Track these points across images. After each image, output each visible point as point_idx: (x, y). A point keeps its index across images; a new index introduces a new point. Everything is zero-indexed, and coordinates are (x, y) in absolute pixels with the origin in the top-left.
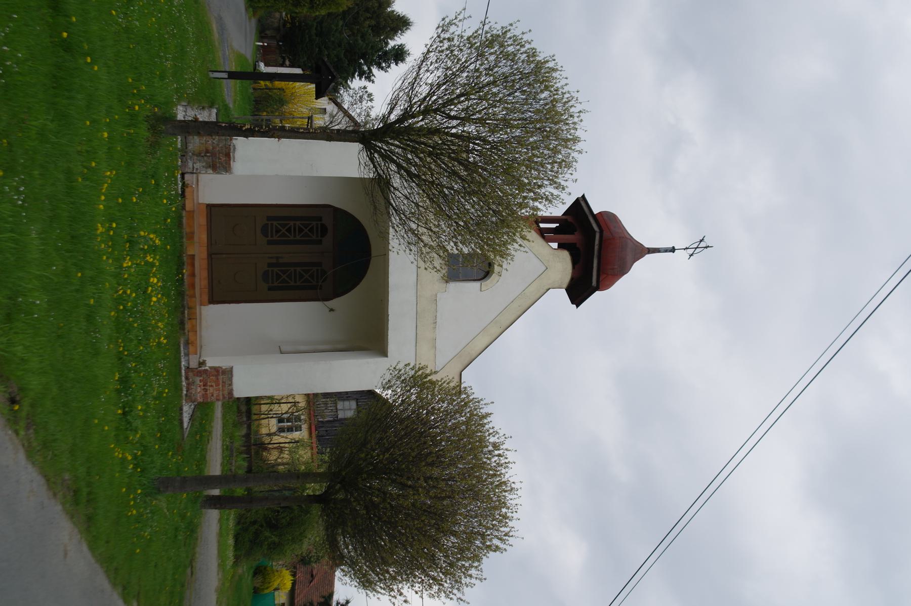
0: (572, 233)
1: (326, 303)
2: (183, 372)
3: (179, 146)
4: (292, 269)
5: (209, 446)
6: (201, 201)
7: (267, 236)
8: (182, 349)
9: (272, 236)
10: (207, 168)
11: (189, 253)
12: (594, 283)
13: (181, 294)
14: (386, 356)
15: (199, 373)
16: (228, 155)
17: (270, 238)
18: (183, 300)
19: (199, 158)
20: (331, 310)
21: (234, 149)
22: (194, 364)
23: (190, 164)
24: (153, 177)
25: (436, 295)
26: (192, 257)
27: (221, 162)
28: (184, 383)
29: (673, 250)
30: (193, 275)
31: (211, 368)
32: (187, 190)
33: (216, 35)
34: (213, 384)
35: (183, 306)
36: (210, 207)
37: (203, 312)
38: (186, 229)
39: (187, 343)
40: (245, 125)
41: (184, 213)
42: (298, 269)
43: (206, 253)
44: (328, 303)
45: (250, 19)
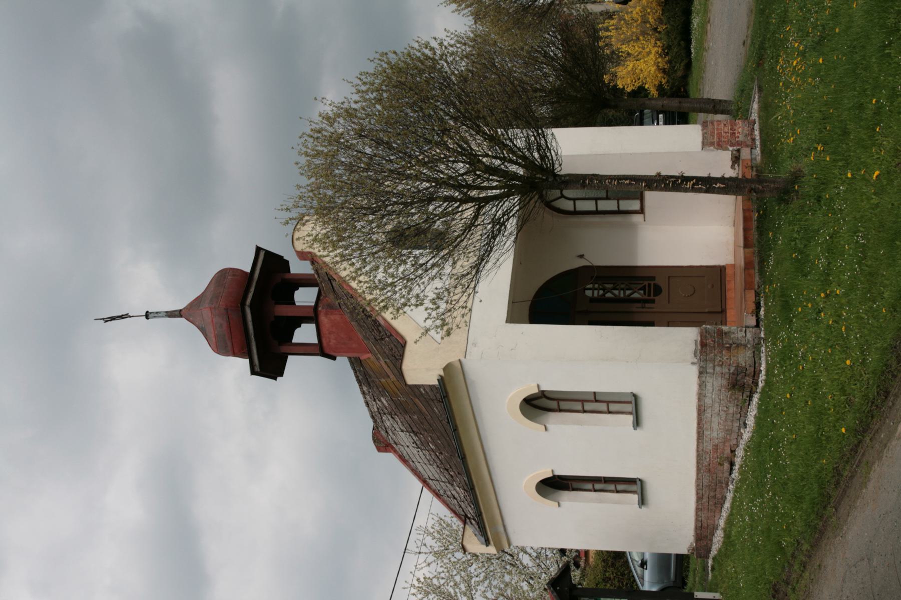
1: (588, 264)
7: (654, 284)
9: (649, 285)
10: (729, 332)
14: (512, 318)
17: (652, 283)
20: (582, 256)
23: (749, 335)
29: (147, 315)
31: (727, 149)
34: (723, 134)
43: (728, 315)
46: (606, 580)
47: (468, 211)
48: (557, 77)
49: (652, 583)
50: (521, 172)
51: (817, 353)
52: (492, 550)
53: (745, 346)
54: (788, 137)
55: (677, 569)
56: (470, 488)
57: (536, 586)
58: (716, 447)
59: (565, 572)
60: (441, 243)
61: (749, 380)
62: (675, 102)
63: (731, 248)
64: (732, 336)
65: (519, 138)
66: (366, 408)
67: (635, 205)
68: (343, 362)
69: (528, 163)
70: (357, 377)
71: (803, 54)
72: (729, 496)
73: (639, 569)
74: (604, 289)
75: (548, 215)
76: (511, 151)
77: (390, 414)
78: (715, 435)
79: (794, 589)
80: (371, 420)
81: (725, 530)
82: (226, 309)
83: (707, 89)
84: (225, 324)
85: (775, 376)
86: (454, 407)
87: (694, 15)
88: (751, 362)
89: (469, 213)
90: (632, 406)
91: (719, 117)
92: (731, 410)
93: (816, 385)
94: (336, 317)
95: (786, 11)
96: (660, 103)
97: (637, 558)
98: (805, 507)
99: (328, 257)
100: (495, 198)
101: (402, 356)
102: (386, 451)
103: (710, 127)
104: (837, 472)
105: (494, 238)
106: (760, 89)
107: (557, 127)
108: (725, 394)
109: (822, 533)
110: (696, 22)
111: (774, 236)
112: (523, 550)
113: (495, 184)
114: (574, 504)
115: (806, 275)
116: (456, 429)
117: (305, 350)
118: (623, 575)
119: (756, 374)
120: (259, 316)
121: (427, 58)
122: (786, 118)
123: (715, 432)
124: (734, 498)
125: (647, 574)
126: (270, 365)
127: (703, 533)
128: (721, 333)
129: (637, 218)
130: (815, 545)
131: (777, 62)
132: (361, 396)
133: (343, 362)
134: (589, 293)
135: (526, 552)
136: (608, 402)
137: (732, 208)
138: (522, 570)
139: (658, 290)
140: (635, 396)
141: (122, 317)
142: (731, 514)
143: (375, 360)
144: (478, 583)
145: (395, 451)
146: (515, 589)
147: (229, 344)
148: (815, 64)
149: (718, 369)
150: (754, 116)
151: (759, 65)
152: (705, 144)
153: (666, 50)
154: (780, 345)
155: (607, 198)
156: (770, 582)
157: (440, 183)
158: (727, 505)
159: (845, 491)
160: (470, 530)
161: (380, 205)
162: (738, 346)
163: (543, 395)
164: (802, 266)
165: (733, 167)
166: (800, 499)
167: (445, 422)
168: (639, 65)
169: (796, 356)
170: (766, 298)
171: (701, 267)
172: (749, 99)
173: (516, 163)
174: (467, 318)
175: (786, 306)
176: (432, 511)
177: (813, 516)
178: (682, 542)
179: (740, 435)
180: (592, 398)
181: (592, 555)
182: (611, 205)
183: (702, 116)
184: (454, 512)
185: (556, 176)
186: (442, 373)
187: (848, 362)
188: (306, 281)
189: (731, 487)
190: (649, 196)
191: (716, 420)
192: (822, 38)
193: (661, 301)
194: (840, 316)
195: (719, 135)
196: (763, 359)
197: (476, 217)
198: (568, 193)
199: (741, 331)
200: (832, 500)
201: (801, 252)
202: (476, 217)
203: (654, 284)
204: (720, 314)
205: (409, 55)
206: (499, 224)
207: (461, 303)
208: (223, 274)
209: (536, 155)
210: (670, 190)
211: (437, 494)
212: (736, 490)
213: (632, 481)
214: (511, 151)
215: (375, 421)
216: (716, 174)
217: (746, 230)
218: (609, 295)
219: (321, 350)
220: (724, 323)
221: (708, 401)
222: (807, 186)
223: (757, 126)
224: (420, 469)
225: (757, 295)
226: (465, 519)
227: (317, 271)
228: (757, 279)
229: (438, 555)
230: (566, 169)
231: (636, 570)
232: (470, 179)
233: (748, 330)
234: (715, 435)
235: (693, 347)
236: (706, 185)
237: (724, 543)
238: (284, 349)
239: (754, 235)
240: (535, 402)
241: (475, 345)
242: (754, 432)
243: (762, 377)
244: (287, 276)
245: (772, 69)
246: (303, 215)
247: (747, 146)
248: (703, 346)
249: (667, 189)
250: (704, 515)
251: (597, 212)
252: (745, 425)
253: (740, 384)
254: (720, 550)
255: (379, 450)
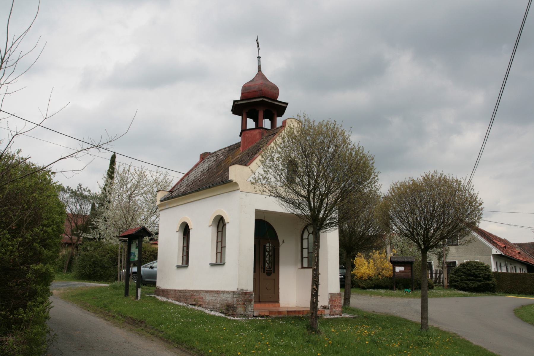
14: (257, 212)
20: (283, 242)
21: (242, 290)
23: (250, 313)
29: (259, 57)
31: (329, 304)
46: (145, 252)
47: (304, 193)
48: (360, 232)
49: (144, 271)
50: (321, 216)
51: (243, 341)
52: (158, 203)
53: (245, 311)
54: (334, 329)
55: (149, 282)
56: (185, 194)
57: (142, 222)
58: (202, 298)
59: (149, 234)
60: (290, 182)
61: (230, 312)
62: (349, 282)
63: (287, 306)
65: (335, 215)
66: (218, 149)
67: (305, 265)
68: (239, 139)
69: (324, 219)
70: (232, 146)
71: (369, 335)
72: (181, 304)
73: (150, 266)
74: (269, 251)
75: (302, 227)
76: (330, 211)
77: (216, 160)
78: (207, 298)
79: (143, 329)
80: (213, 151)
81: (167, 302)
82: (261, 90)
83: (354, 296)
84: (255, 89)
85: (233, 323)
86: (220, 187)
87: (385, 290)
88: (238, 313)
89: (303, 193)
90: (220, 262)
91: (343, 301)
92: (217, 305)
93: (229, 340)
94: (258, 137)
95: (387, 328)
96: (349, 275)
97: (154, 265)
98: (177, 335)
99: (283, 133)
100: (310, 204)
101: (241, 164)
102: (200, 158)
103: (339, 297)
104: (192, 348)
105: (292, 204)
106: (354, 318)
107: (339, 232)
108: (225, 302)
109: (166, 342)
110: (382, 291)
111: (292, 324)
112: (159, 220)
113: (316, 204)
114: (177, 238)
115: (276, 336)
116: (210, 187)
117: (244, 123)
118: (147, 259)
119: (233, 315)
120: (258, 104)
121: (371, 175)
122: (342, 329)
123: (208, 298)
124: (180, 306)
125: (148, 269)
126: (237, 108)
127: (165, 293)
128: (251, 301)
129: (300, 266)
130: (161, 338)
131: (366, 325)
132: (224, 147)
133: (239, 139)
134: (268, 245)
135: (157, 218)
136: (221, 253)
137: (303, 306)
138: (149, 216)
139: (269, 274)
140: (224, 264)
141: (258, 47)
142: (173, 304)
143: (239, 154)
144: (144, 197)
145: (200, 162)
146: (140, 213)
147: (247, 91)
148: (365, 340)
149: (235, 299)
150: (343, 315)
151: (365, 317)
153: (370, 278)
154: (246, 325)
155: (308, 253)
156: (145, 320)
157: (316, 181)
158: (177, 303)
159: (184, 351)
160: (166, 194)
161: (306, 155)
162: (245, 308)
163: (224, 225)
164: (280, 335)
165: (321, 306)
166: (181, 333)
167: (213, 183)
168: (364, 267)
169: (241, 332)
170: (265, 320)
171: (279, 293)
172: (351, 313)
173: (325, 213)
174: (258, 192)
175: (262, 328)
176: (174, 178)
177: (174, 338)
178: (161, 284)
179: (207, 309)
180: (223, 246)
181: (155, 246)
182: (305, 254)
183: (343, 294)
184: (174, 187)
185: (319, 230)
186: (234, 181)
187: (239, 353)
188: (273, 124)
189: (185, 304)
190: (310, 271)
191: (214, 298)
192: (376, 343)
193: (264, 276)
194: (259, 350)
195: (335, 301)
196: (239, 318)
197: (302, 196)
198: (311, 236)
200: (180, 346)
201: (286, 334)
202: (302, 196)
204: (259, 300)
205: (371, 169)
206: (298, 206)
207: (265, 189)
208: (276, 89)
209: (328, 222)
210: (313, 279)
211: (182, 180)
212: (184, 307)
213: (187, 263)
214: (330, 211)
215: (213, 153)
216: (319, 299)
217: (295, 312)
218: (267, 253)
219: (244, 130)
220: (255, 302)
221: (222, 295)
222: (313, 337)
223: (339, 316)
224: (193, 172)
225: (267, 316)
226: (171, 191)
227: (278, 128)
228: (274, 316)
229: (156, 181)
230: (322, 234)
231: (149, 265)
232: (318, 193)
234: (207, 298)
235: (245, 289)
236: (315, 294)
237: (161, 301)
238: (244, 115)
239: (293, 315)
240: (221, 221)
241: (246, 196)
242: (209, 314)
243: (232, 318)
244: (276, 116)
245: (363, 323)
246: (301, 123)
248: (245, 293)
249: (313, 277)
250: (173, 293)
251: (302, 248)
252: (211, 311)
253: (229, 309)
254: (158, 299)
255: (201, 155)
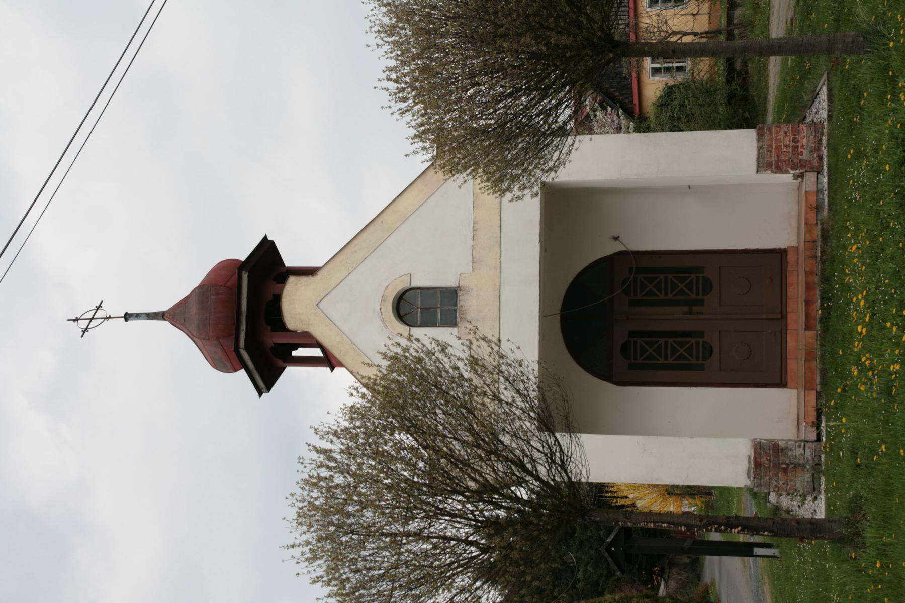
0: (277, 345)
1: (625, 249)
2: (825, 168)
3: (823, 479)
4: (670, 297)
5: (790, 14)
6: (795, 392)
7: (703, 277)
8: (826, 201)
9: (698, 278)
10: (786, 448)
11: (811, 333)
12: (245, 276)
13: (826, 279)
15: (802, 165)
16: (758, 465)
18: (823, 271)
19: (796, 461)
20: (616, 238)
22: (811, 177)
24: (859, 465)
25: (473, 270)
26: (808, 327)
27: (768, 459)
28: (825, 152)
29: (127, 317)
30: (808, 303)
31: (787, 172)
32: (813, 418)
33: (767, 589)
34: (784, 149)
35: (823, 262)
36: (781, 384)
37: (795, 238)
38: (816, 365)
39: (818, 208)
40: (738, 532)
41: (818, 388)
42: (661, 361)
44: (617, 247)
45: (713, 583)
53: (804, 466)
64: (790, 453)
152: (763, 165)
162: (797, 466)
199: (799, 446)
203: (703, 277)
233: (807, 445)
247: (812, 170)
